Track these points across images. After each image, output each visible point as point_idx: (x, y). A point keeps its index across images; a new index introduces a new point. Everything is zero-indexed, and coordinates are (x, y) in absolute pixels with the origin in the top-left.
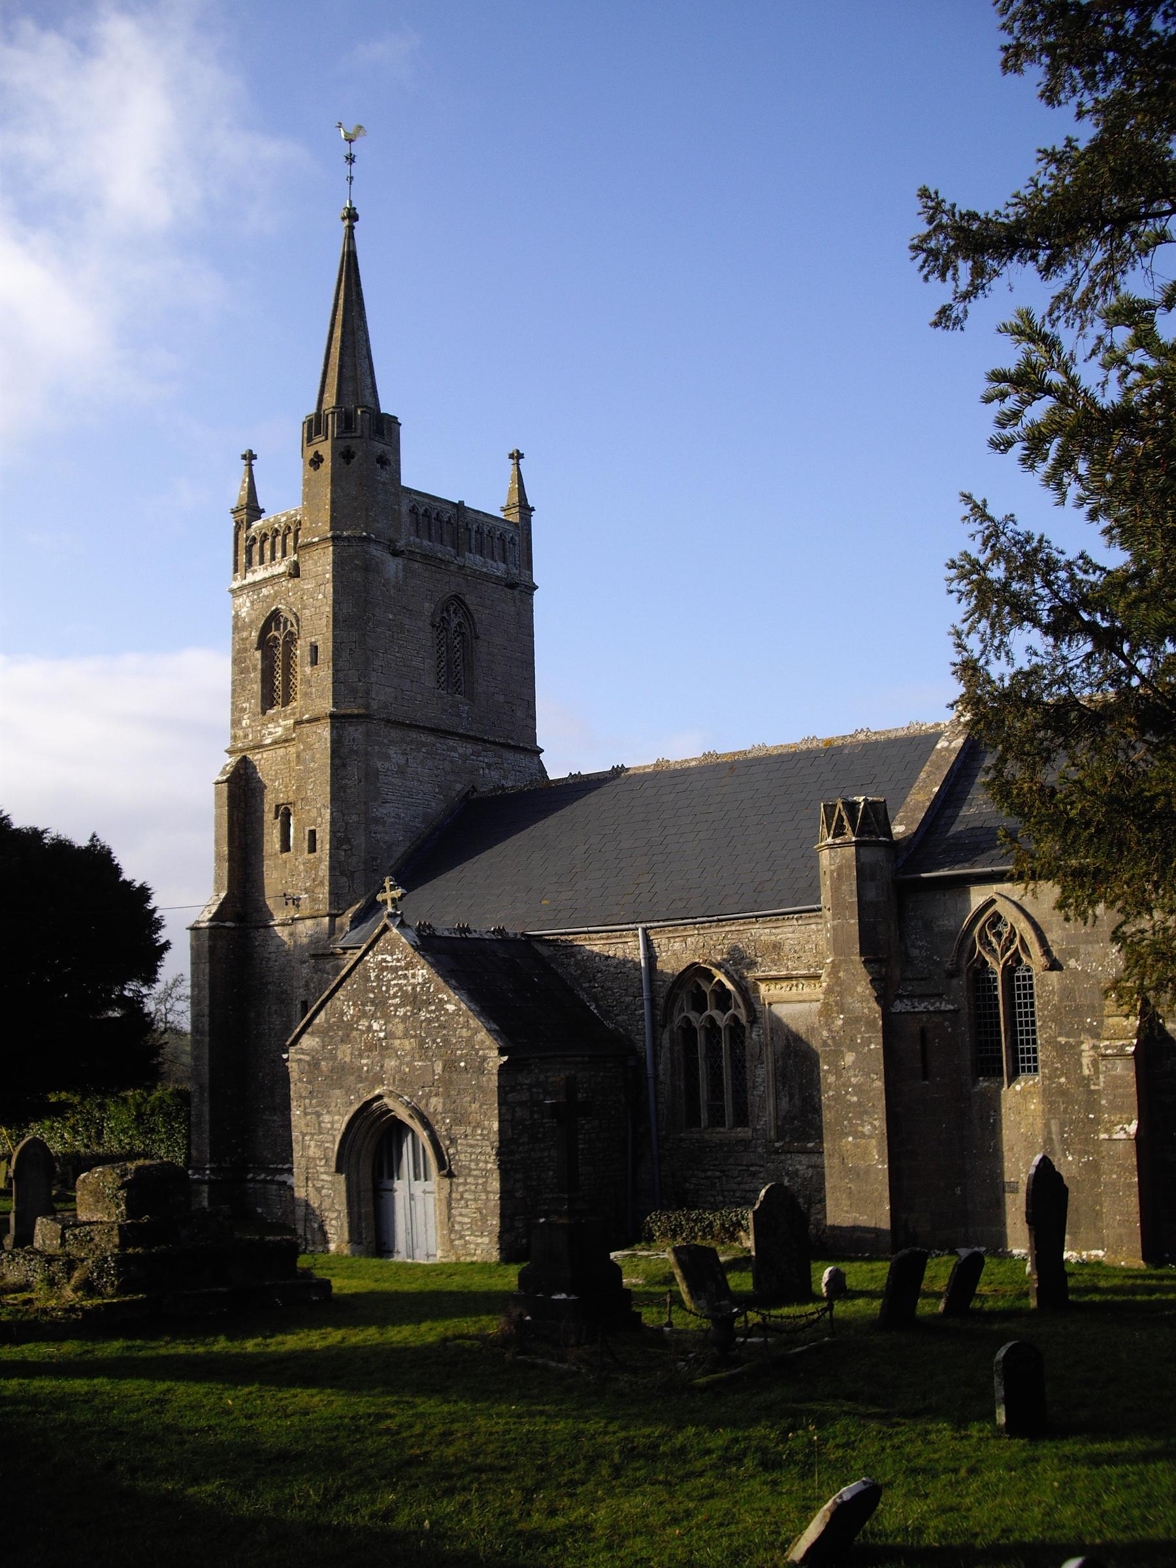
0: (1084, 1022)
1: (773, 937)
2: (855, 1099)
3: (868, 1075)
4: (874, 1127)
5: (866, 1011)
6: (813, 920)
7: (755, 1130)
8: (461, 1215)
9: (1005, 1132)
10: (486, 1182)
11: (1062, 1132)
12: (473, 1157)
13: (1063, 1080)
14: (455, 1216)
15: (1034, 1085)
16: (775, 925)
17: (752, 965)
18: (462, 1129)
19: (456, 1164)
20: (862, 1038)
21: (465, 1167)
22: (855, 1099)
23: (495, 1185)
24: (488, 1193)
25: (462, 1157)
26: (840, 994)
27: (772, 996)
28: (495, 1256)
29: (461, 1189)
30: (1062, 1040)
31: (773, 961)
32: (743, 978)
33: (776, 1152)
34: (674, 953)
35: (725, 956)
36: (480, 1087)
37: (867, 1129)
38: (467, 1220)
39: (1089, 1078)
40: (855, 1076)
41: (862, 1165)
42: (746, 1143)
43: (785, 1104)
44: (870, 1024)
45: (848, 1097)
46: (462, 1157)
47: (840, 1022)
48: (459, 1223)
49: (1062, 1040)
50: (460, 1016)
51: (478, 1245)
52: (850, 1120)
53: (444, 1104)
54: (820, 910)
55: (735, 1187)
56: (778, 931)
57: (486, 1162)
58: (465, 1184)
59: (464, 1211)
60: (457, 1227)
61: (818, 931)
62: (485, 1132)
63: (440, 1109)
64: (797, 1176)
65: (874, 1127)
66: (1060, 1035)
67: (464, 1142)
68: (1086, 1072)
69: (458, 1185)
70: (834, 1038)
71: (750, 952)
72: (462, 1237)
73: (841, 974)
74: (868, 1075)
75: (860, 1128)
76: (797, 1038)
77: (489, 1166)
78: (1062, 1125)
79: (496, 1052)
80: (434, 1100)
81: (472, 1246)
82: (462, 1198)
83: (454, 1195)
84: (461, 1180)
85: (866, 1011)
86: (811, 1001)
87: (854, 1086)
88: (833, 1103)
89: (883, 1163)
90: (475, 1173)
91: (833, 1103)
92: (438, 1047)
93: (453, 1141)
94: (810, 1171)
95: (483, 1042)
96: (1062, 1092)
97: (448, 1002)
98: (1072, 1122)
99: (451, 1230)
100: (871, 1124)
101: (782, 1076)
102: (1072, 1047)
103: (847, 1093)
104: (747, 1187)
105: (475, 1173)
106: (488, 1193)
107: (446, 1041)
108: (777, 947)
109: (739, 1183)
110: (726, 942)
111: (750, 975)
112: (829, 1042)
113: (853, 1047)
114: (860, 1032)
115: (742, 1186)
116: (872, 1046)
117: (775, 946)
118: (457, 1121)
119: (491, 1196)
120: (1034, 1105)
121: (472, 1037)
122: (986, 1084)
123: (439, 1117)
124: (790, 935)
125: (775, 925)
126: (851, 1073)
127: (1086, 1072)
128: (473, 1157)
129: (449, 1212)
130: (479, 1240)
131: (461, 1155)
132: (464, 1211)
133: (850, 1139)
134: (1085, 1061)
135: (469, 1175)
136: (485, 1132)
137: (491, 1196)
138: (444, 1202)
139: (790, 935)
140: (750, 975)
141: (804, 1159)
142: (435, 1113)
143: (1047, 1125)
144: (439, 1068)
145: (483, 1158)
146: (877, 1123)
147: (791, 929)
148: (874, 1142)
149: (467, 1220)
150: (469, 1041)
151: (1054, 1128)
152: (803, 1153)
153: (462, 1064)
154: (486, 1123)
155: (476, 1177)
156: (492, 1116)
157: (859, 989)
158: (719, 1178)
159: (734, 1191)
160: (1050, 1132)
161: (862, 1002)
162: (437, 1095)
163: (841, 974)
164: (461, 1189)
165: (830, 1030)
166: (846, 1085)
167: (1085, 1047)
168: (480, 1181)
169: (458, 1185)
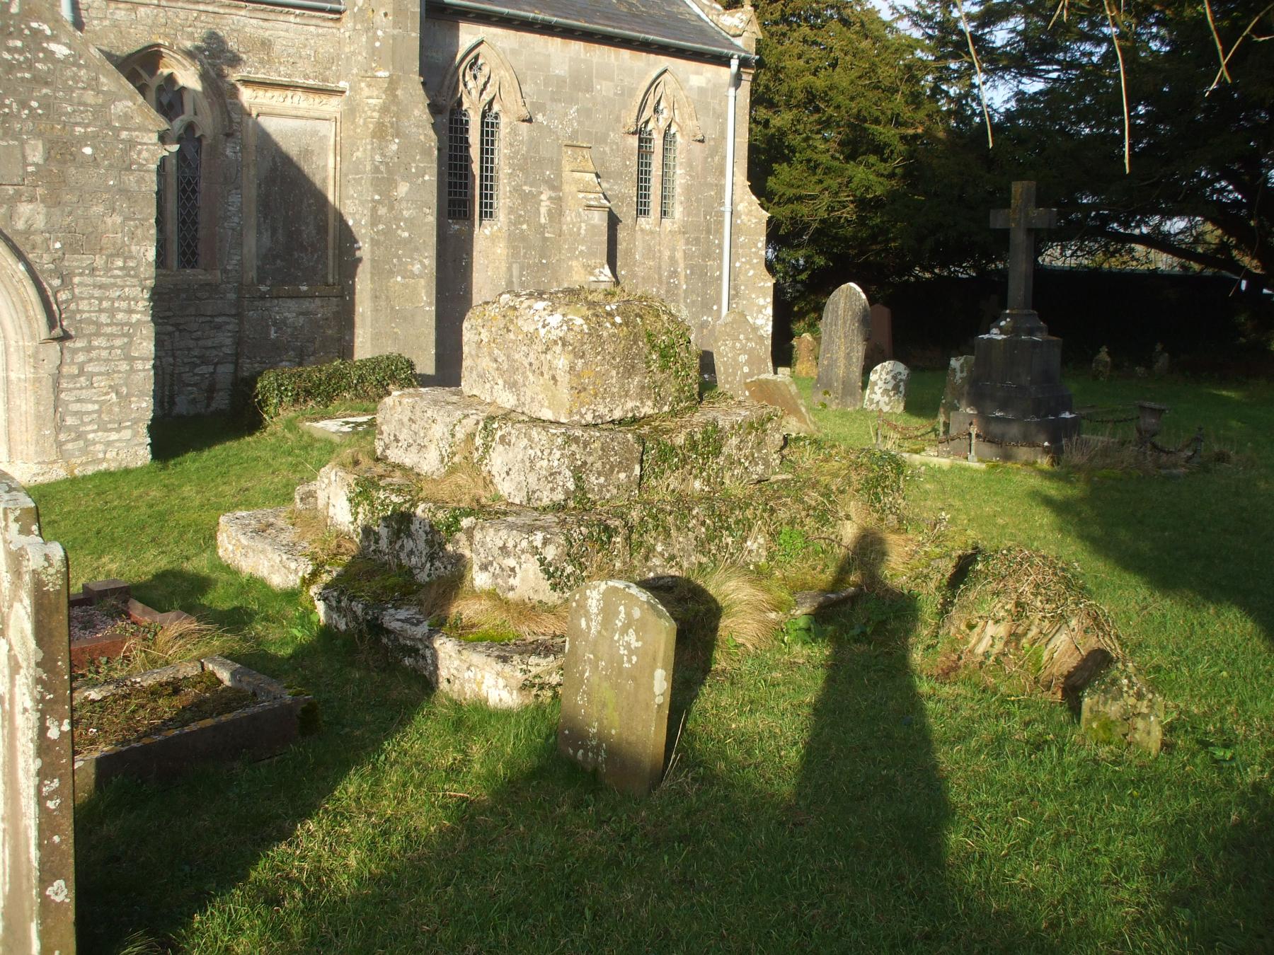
0: (544, 173)
1: (261, 31)
2: (406, 234)
3: (420, 208)
4: (424, 266)
5: (422, 137)
6: (314, 21)
7: (225, 271)
8: (79, 401)
9: (475, 275)
10: (130, 343)
11: (521, 275)
12: (105, 304)
13: (525, 227)
14: (67, 403)
15: (500, 230)
16: (306, 21)
17: (235, 61)
18: (86, 260)
19: (71, 318)
20: (417, 167)
21: (89, 322)
22: (406, 234)
23: (146, 346)
24: (130, 359)
25: (84, 305)
26: (397, 115)
27: (262, 105)
28: (142, 455)
29: (81, 357)
30: (527, 188)
31: (261, 62)
32: (221, 76)
33: (262, 298)
34: (116, 24)
35: (199, 43)
36: (124, 191)
37: (417, 268)
38: (90, 407)
39: (544, 227)
40: (408, 209)
41: (409, 306)
42: (212, 288)
43: (266, 240)
44: (426, 152)
45: (399, 232)
46: (84, 305)
47: (394, 147)
48: (76, 413)
49: (527, 188)
50: (80, 66)
51: (109, 444)
52: (399, 258)
53: (49, 216)
54: (339, 12)
55: (191, 344)
56: (265, 24)
57: (130, 311)
58: (89, 349)
59: (84, 394)
60: (70, 421)
61: (318, 35)
62: (131, 264)
63: (40, 222)
64: (285, 325)
65: (424, 266)
66: (525, 184)
67: (89, 280)
68: (543, 221)
69: (75, 351)
70: (387, 164)
71: (232, 44)
72: (80, 436)
73: (399, 92)
74: (420, 208)
75: (410, 267)
76: (286, 160)
77: (135, 317)
78: (522, 269)
79: (154, 138)
80: (25, 209)
81: (99, 447)
82: (82, 372)
83: (65, 370)
84: (79, 344)
85: (422, 137)
86: (307, 118)
87: (406, 220)
88: (382, 238)
89: (429, 304)
90: (109, 330)
91: (382, 238)
92: (32, 114)
93: (66, 279)
94: (301, 319)
95: (127, 117)
96: (523, 237)
97: (54, 38)
98: (529, 266)
99: (59, 428)
100: (421, 262)
101: (265, 206)
102: (534, 196)
103: (399, 227)
104: (209, 343)
105: (109, 330)
106: (130, 359)
107: (46, 104)
108: (266, 45)
109: (197, 339)
110: (198, 24)
111: (234, 76)
112: (382, 168)
113: (407, 177)
114: (414, 161)
115: (201, 343)
116: (427, 178)
117: (263, 43)
118: (72, 247)
119: (139, 365)
120: (501, 250)
121: (105, 105)
122: (457, 227)
123: (38, 239)
124: (282, 34)
125: (306, 21)
126: (404, 205)
127: (543, 221)
128: (105, 304)
129: (57, 398)
130: (114, 436)
131: (83, 301)
132: (84, 394)
133: (399, 279)
134: (543, 210)
135: (98, 334)
136: (131, 264)
137: (139, 365)
138: (47, 382)
139: (282, 34)
140: (234, 76)
141: (292, 304)
142: (28, 232)
143: (509, 269)
144: (36, 154)
145: (124, 305)
146: (426, 262)
147: (285, 25)
148: (422, 282)
149: (90, 407)
150: (100, 111)
151: (515, 272)
152: (291, 297)
153: (88, 151)
154: (133, 248)
155: (111, 336)
156: (145, 238)
157: (416, 112)
158: (170, 334)
159: (189, 349)
160: (511, 276)
161: (418, 127)
162: (32, 200)
163: (399, 92)
164: (81, 357)
165: (383, 155)
166: (397, 219)
167: (544, 197)
168: (118, 342)
169: (75, 351)
